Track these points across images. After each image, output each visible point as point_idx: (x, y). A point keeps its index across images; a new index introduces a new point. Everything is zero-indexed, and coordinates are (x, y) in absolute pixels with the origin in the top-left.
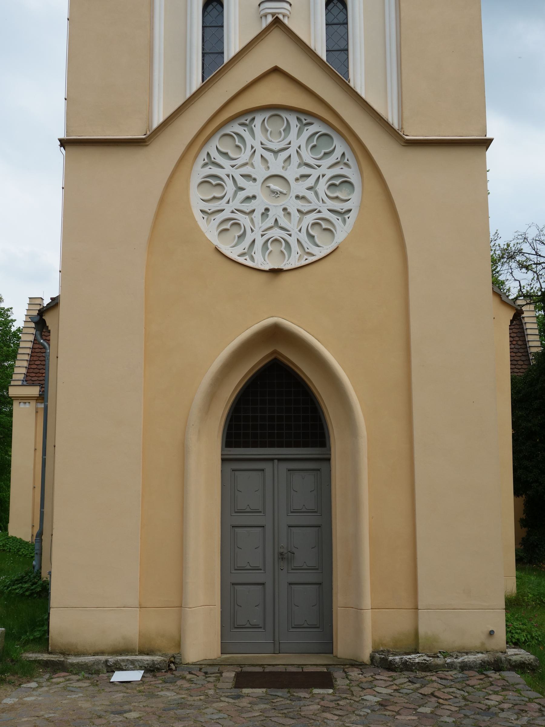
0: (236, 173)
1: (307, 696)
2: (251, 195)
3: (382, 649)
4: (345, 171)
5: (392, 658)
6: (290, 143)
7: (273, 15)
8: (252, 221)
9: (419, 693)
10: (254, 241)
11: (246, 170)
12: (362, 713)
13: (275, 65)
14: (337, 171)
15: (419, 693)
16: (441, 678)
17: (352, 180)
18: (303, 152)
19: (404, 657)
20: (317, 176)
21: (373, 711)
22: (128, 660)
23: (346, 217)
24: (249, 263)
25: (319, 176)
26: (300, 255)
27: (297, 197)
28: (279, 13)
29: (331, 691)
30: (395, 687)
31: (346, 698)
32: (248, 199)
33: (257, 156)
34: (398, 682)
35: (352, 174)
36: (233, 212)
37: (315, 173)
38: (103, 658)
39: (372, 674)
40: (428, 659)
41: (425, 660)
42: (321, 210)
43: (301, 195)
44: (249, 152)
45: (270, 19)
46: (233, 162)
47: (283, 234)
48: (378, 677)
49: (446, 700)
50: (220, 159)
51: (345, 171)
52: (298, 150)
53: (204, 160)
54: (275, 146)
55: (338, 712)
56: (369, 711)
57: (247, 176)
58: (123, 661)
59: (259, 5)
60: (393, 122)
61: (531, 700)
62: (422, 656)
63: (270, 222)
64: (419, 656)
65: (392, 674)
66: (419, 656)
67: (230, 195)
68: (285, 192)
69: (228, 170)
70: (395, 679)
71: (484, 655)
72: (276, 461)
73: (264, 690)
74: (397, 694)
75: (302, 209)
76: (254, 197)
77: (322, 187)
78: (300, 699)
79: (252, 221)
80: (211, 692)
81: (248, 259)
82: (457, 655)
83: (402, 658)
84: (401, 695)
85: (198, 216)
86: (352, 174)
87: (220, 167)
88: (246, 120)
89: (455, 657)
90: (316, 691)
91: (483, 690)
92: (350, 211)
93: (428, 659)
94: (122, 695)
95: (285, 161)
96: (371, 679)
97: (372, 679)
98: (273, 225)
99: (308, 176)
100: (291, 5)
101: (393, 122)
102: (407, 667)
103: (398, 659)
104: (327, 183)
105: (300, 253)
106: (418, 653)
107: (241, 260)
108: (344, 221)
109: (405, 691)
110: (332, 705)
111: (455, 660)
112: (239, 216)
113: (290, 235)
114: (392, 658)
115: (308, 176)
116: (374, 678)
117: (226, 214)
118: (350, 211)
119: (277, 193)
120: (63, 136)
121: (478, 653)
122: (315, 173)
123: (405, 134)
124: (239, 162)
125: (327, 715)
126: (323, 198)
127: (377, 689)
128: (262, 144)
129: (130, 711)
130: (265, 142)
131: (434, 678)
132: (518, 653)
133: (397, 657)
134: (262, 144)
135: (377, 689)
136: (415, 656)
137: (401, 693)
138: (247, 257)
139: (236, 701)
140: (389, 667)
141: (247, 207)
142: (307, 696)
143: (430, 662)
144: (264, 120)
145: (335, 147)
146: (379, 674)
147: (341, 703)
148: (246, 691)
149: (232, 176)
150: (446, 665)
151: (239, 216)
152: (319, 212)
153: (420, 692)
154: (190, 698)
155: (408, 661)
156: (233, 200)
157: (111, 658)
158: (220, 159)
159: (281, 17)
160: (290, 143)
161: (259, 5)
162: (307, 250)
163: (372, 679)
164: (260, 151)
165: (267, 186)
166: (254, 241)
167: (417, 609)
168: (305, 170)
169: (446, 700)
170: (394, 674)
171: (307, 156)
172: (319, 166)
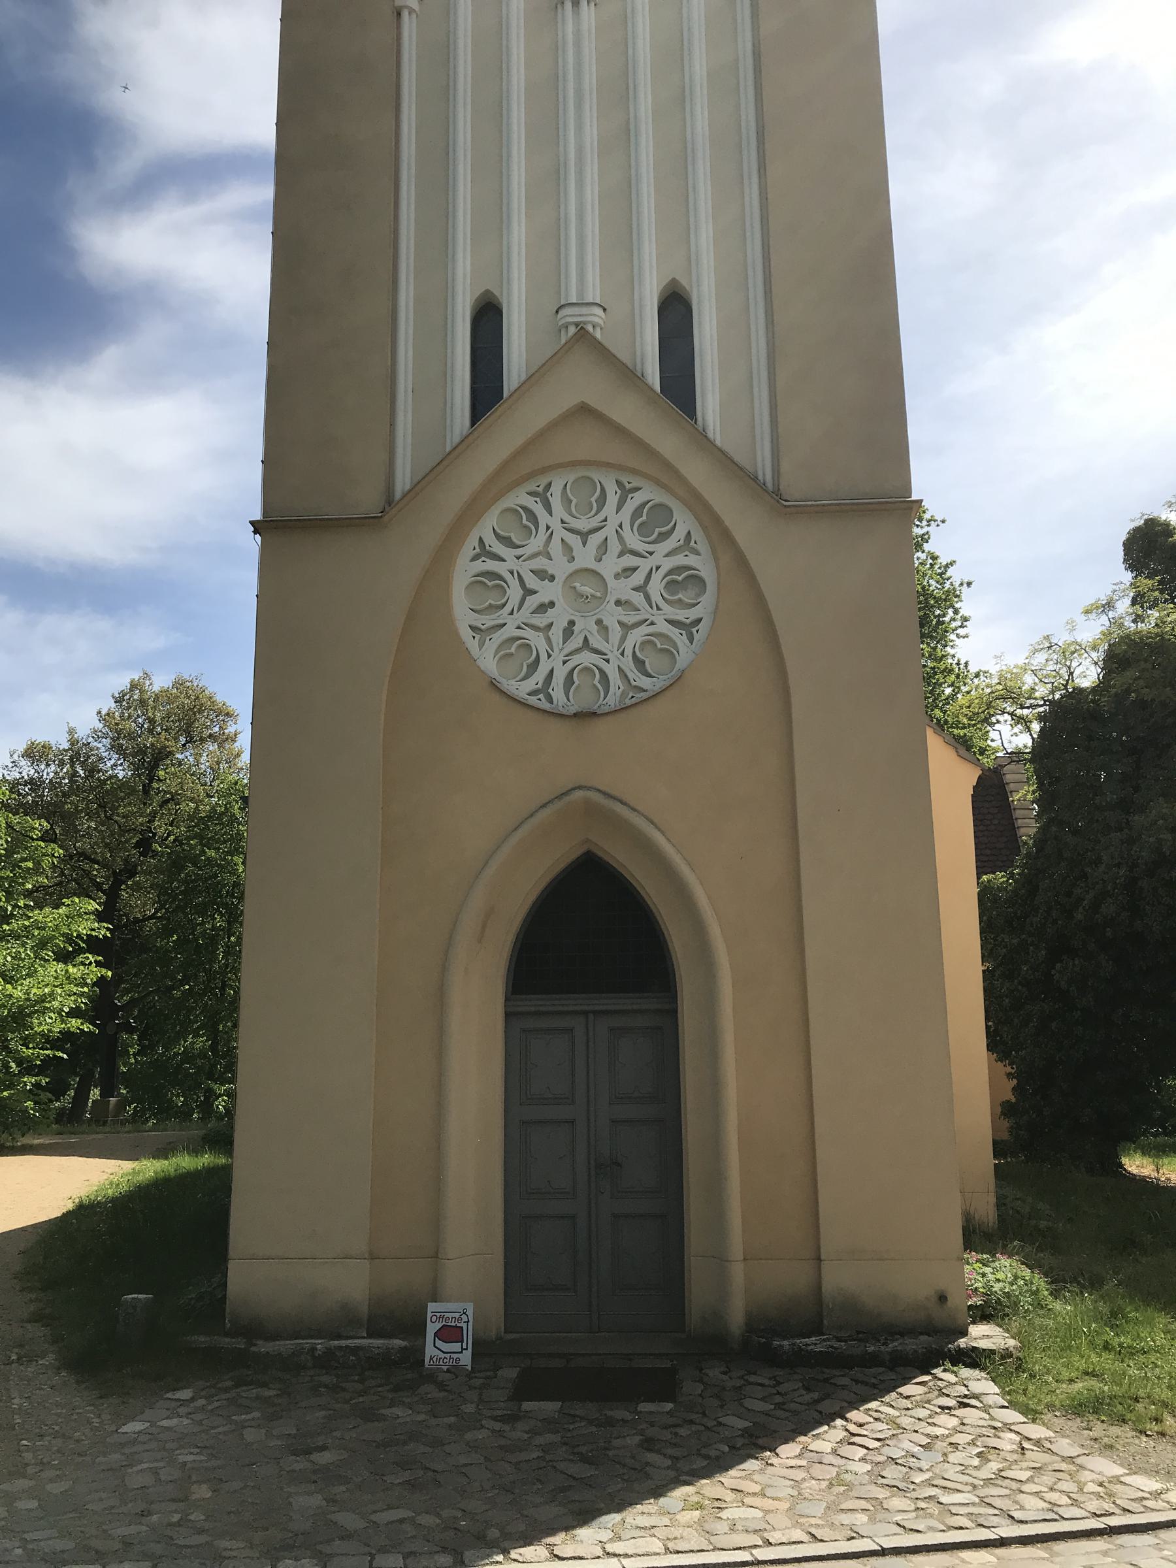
0: (525, 569)
1: (628, 1416)
2: (547, 601)
3: (762, 1327)
4: (692, 560)
5: (778, 1343)
6: (605, 520)
7: (577, 324)
8: (549, 641)
9: (817, 1411)
10: (552, 671)
11: (540, 563)
12: (713, 1453)
13: (484, 290)
14: (680, 560)
15: (817, 1411)
16: (857, 1382)
17: (703, 574)
18: (627, 533)
19: (798, 1341)
20: (650, 568)
21: (732, 1448)
22: (347, 1347)
23: (694, 630)
24: (544, 705)
25: (652, 569)
26: (623, 691)
27: (618, 603)
28: (585, 323)
29: (669, 1406)
30: (778, 1399)
31: (692, 1422)
32: (543, 608)
33: (556, 540)
34: (782, 1388)
35: (702, 564)
36: (519, 628)
37: (645, 565)
38: (307, 1343)
39: (743, 1372)
40: (836, 1344)
41: (832, 1347)
42: (656, 621)
43: (623, 598)
44: (542, 535)
45: (572, 330)
46: (519, 552)
47: (596, 659)
48: (752, 1378)
49: (861, 1425)
50: (499, 548)
51: (692, 560)
52: (619, 529)
53: (474, 549)
54: (583, 524)
55: (670, 1451)
56: (726, 1449)
57: (541, 575)
58: (340, 1348)
59: (557, 312)
60: (764, 480)
61: (1008, 1427)
62: (828, 1340)
63: (576, 642)
64: (824, 1340)
65: (777, 1373)
66: (824, 1340)
67: (514, 601)
68: (598, 594)
69: (511, 563)
70: (779, 1383)
71: (931, 1338)
72: (591, 1016)
73: (557, 1405)
74: (779, 1413)
75: (625, 620)
76: (552, 604)
77: (656, 587)
78: (610, 1422)
79: (549, 641)
80: (470, 1408)
81: (543, 699)
82: (886, 1339)
83: (793, 1344)
84: (787, 1414)
85: (466, 634)
86: (702, 564)
87: (500, 559)
88: (538, 486)
89: (882, 1342)
90: (645, 1407)
91: (925, 1405)
92: (699, 620)
93: (836, 1344)
94: (323, 1413)
95: (625, 570)
96: (739, 1383)
97: (742, 1382)
98: (581, 645)
99: (635, 569)
100: (605, 310)
101: (764, 480)
102: (801, 1359)
103: (787, 1347)
104: (664, 578)
105: (622, 688)
106: (823, 1334)
107: (532, 700)
108: (691, 639)
109: (793, 1406)
110: (666, 1435)
111: (883, 1348)
112: (528, 633)
113: (608, 661)
114: (778, 1343)
115: (635, 569)
116: (747, 1380)
117: (510, 631)
118: (699, 620)
119: (587, 597)
120: (258, 516)
121: (921, 1334)
122: (645, 565)
123: (785, 498)
124: (527, 551)
125: (651, 1457)
126: (658, 604)
127: (748, 1403)
128: (563, 522)
129: (323, 1448)
130: (567, 518)
131: (845, 1381)
132: (990, 1334)
133: (786, 1343)
134: (563, 522)
135: (748, 1403)
136: (816, 1340)
137: (787, 1411)
138: (541, 696)
139: (507, 1428)
140: (773, 1359)
141: (540, 621)
142: (628, 1416)
143: (839, 1351)
144: (566, 485)
145: (675, 524)
146: (755, 1374)
147: (683, 1432)
148: (527, 1406)
149: (518, 572)
150: (867, 1357)
151: (528, 633)
152: (652, 624)
153: (819, 1409)
154: (434, 1422)
155: (802, 1350)
156: (519, 609)
157: (321, 1344)
158: (499, 548)
159: (590, 328)
160: (605, 520)
161: (557, 312)
162: (634, 683)
163: (742, 1382)
164: (560, 533)
165: (571, 587)
166: (552, 671)
167: (819, 1259)
168: (630, 561)
169: (861, 1425)
170: (779, 1372)
171: (634, 541)
172: (651, 553)
